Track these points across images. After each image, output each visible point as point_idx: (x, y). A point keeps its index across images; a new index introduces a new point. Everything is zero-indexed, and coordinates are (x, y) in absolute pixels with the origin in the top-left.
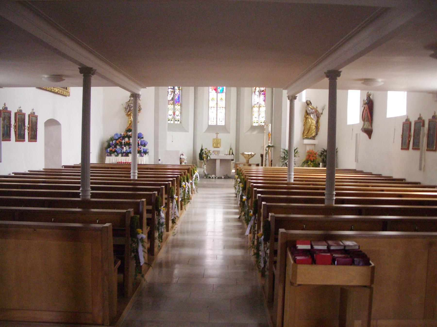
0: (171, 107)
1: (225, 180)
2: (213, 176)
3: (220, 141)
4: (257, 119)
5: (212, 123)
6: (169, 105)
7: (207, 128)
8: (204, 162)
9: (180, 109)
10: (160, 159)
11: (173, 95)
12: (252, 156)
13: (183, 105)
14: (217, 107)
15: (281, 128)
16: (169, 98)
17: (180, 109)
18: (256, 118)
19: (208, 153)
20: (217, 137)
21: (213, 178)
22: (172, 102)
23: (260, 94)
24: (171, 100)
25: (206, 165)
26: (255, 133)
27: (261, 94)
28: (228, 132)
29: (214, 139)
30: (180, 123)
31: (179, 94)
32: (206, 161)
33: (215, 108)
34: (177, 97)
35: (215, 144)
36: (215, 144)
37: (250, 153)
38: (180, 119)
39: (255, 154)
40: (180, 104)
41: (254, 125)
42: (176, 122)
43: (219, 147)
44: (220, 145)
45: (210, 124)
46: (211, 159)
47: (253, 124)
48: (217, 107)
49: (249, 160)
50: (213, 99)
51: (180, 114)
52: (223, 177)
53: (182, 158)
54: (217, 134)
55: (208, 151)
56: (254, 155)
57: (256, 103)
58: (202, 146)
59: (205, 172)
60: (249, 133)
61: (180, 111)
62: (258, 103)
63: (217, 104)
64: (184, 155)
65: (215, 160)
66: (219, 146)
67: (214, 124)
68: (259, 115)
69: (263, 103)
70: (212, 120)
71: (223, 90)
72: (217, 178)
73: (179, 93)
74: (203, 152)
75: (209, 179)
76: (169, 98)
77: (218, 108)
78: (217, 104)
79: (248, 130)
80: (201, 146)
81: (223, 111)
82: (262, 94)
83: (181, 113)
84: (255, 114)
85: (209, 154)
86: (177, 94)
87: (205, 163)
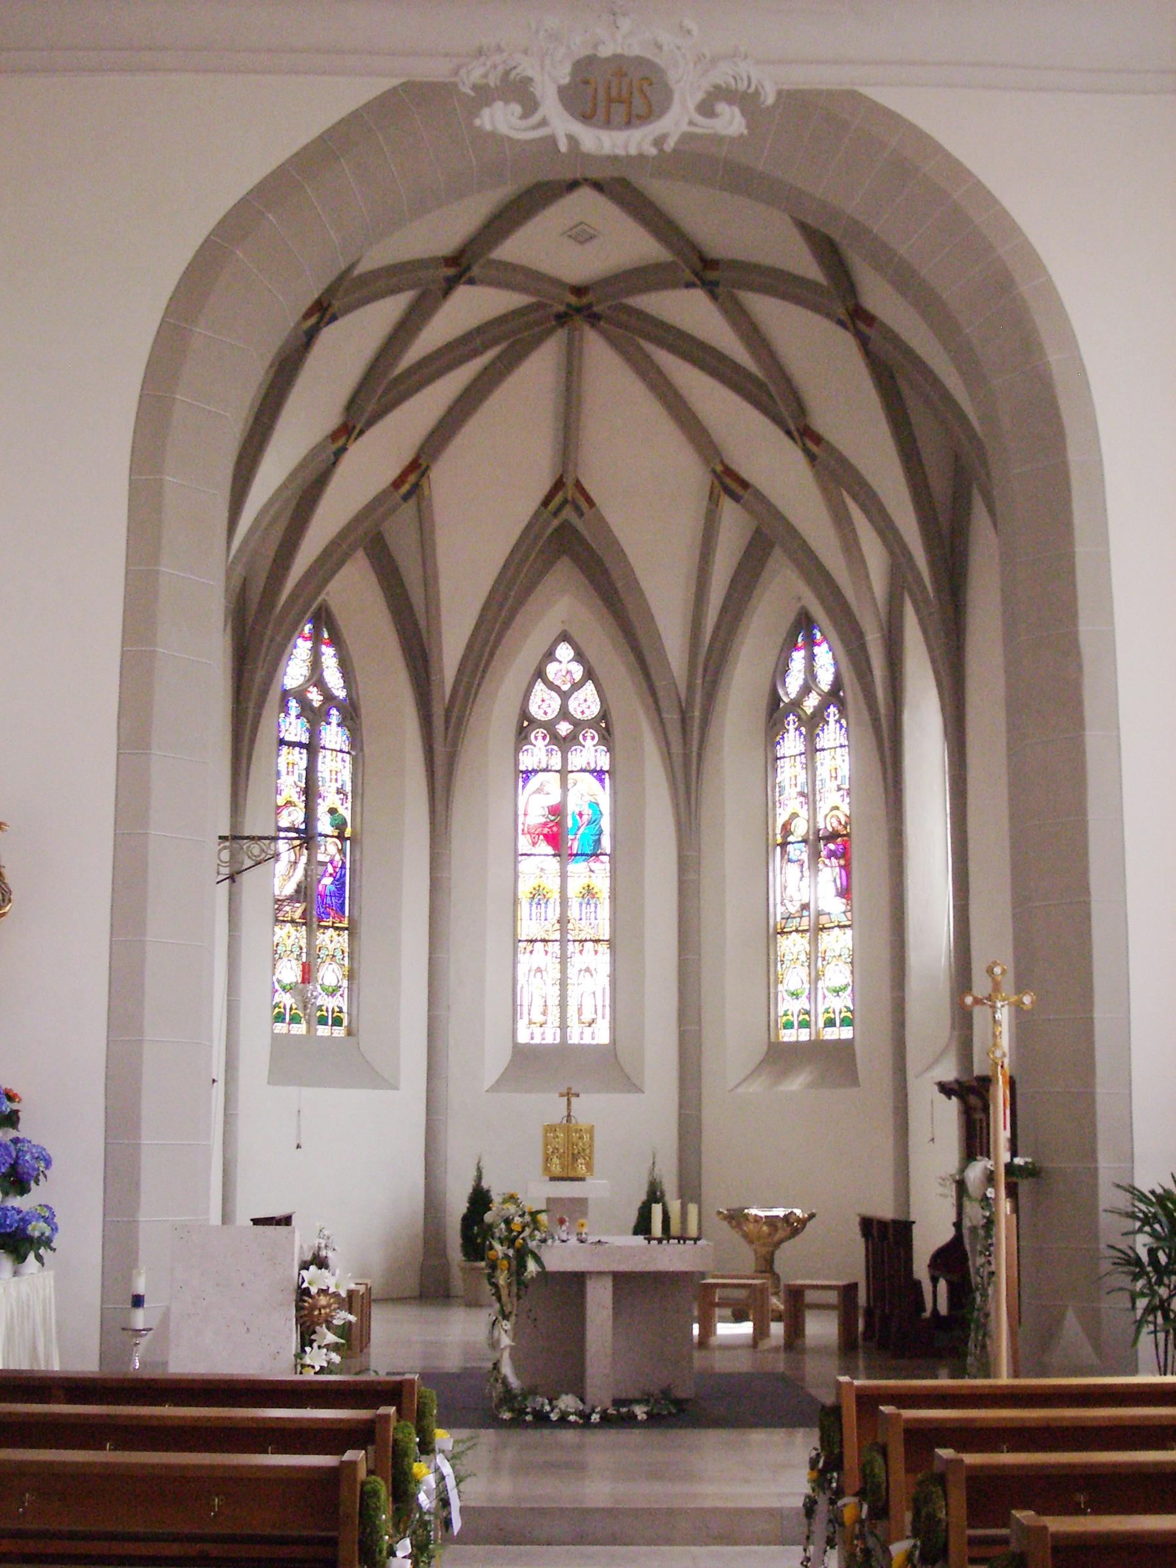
0: (290, 937)
1: (655, 1436)
2: (567, 1402)
3: (586, 1137)
4: (803, 1003)
5: (538, 1031)
6: (277, 929)
7: (509, 1058)
8: (499, 1299)
9: (346, 955)
10: (141, 1290)
11: (306, 870)
12: (793, 1227)
13: (364, 929)
14: (563, 942)
15: (1090, 1022)
16: (282, 887)
17: (346, 950)
18: (795, 995)
19: (527, 1231)
20: (569, 1115)
21: (563, 1421)
22: (299, 908)
23: (815, 855)
24: (291, 899)
25: (513, 1318)
26: (796, 1083)
27: (824, 853)
28: (633, 1087)
29: (551, 1129)
30: (349, 1033)
31: (344, 863)
32: (514, 1289)
33: (555, 948)
34: (331, 879)
35: (556, 1160)
36: (556, 1160)
37: (780, 1212)
38: (345, 1009)
39: (812, 1216)
40: (345, 924)
41: (788, 1036)
42: (323, 1031)
43: (582, 1179)
44: (589, 1167)
45: (523, 1038)
46: (545, 1276)
47: (777, 1035)
48: (563, 942)
49: (772, 1254)
50: (538, 896)
51: (345, 983)
52: (640, 1411)
53: (314, 1290)
54: (569, 1095)
55: (527, 1218)
56: (803, 1222)
57: (793, 909)
58: (479, 1170)
59: (507, 1369)
60: (757, 1087)
61: (346, 962)
62: (805, 907)
63: (563, 921)
64: (331, 1263)
65: (576, 1281)
66: (582, 1169)
67: (551, 1036)
68: (818, 978)
69: (835, 907)
70: (537, 1017)
71: (598, 842)
72: (595, 1418)
73: (338, 858)
74: (490, 1227)
75: (533, 1435)
76: (282, 887)
77: (571, 948)
78: (563, 921)
79: (756, 1071)
80: (474, 1173)
81: (601, 961)
82: (831, 854)
83: (351, 976)
84: (794, 977)
85: (532, 1236)
86: (331, 862)
87: (508, 1309)
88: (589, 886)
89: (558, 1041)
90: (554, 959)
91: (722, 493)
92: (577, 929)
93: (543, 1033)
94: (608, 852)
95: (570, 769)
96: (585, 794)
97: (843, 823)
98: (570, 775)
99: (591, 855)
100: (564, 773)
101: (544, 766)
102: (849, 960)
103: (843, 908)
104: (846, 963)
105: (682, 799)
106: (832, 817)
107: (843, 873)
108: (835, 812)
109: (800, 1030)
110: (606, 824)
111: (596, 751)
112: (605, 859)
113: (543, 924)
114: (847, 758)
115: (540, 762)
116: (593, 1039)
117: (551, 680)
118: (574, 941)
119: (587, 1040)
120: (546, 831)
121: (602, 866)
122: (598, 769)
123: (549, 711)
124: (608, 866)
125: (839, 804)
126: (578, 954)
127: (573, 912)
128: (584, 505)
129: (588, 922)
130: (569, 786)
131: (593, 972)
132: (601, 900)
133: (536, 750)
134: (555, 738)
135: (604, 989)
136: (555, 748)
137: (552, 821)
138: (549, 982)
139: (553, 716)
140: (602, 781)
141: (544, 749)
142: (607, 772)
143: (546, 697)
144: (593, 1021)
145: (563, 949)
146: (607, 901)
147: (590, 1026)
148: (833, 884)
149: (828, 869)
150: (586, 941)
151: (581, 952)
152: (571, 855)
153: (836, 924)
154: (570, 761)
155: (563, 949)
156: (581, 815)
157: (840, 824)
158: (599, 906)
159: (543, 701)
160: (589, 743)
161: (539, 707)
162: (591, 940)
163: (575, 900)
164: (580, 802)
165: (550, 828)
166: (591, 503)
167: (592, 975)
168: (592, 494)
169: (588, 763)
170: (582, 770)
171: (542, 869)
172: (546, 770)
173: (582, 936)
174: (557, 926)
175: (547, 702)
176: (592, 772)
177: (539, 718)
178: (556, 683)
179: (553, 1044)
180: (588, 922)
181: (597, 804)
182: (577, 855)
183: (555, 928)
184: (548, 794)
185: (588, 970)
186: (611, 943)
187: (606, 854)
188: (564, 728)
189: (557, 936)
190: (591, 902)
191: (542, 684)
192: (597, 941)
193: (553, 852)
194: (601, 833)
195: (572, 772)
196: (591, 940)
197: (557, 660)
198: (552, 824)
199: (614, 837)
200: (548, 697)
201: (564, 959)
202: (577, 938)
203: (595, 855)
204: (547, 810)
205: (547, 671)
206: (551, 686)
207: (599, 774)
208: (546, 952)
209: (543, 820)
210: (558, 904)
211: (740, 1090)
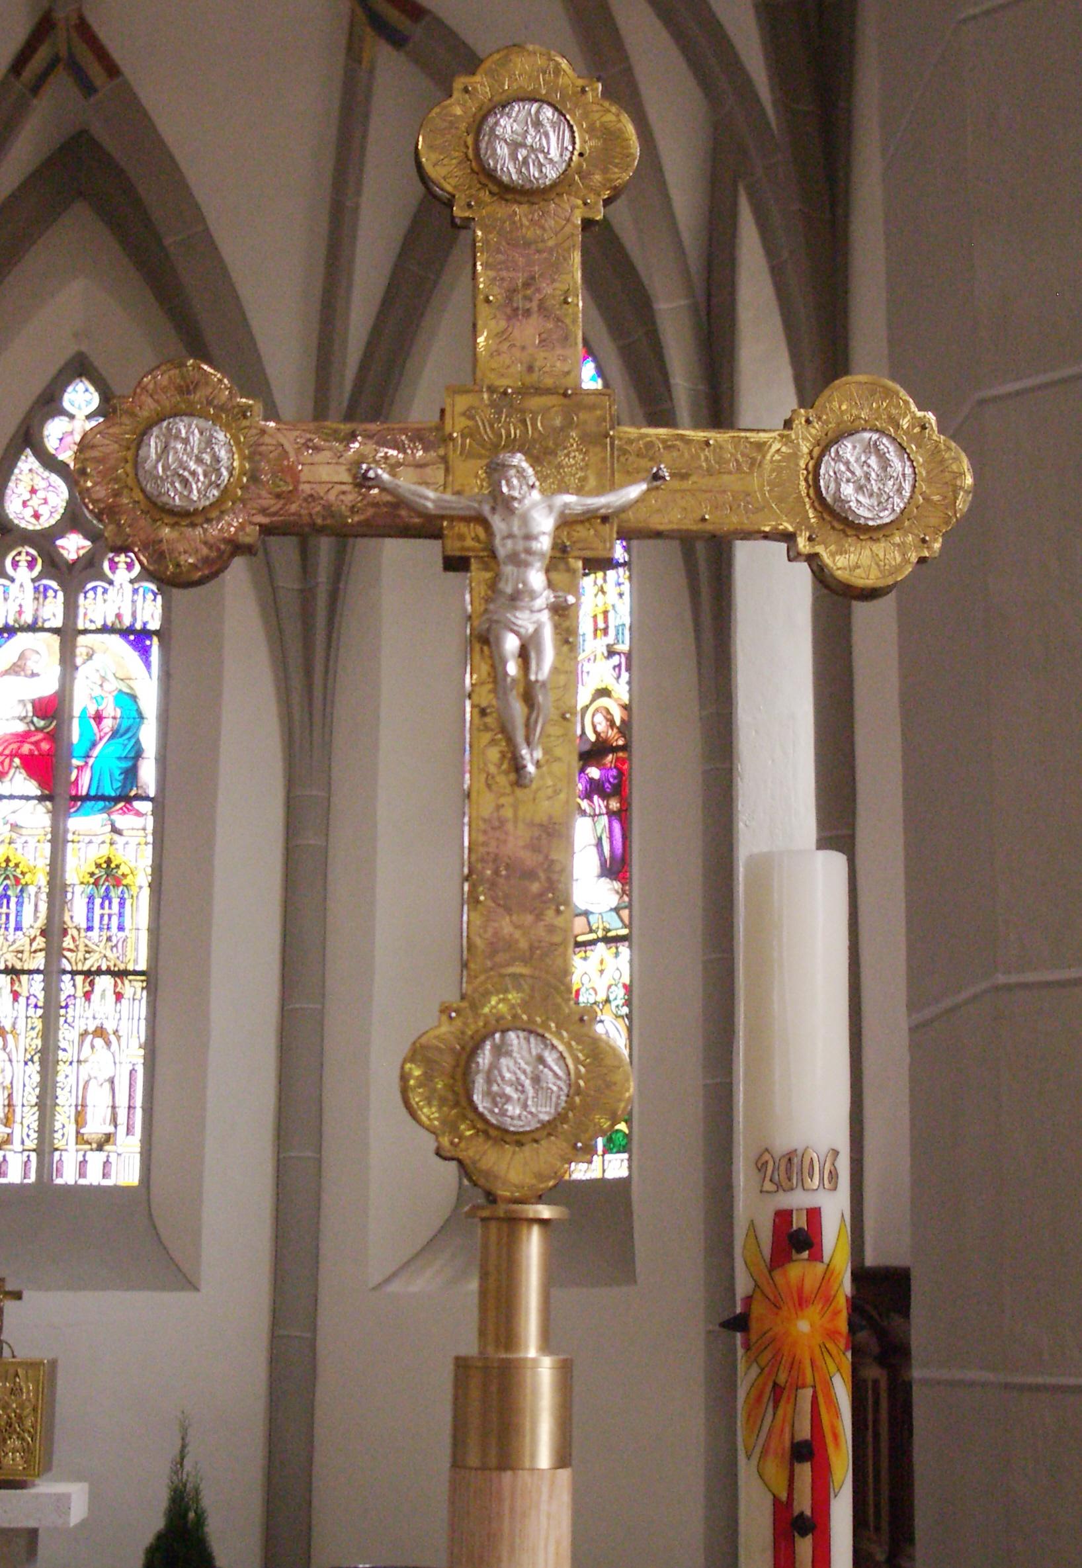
14: (51, 974)
63: (54, 931)
71: (131, 774)
78: (54, 931)
88: (109, 861)
89: (32, 1179)
90: (31, 1011)
91: (369, 32)
92: (82, 948)
93: (107, 1163)
94: (152, 794)
95: (81, 626)
96: (110, 677)
97: (618, 723)
98: (81, 640)
99: (116, 800)
100: (68, 634)
101: (28, 618)
102: (625, 1010)
103: (614, 900)
104: (617, 1016)
105: (297, 683)
106: (597, 710)
107: (617, 827)
108: (603, 702)
109: (607, 1157)
110: (149, 736)
111: (135, 591)
112: (145, 807)
113: (11, 938)
114: (626, 588)
115: (20, 613)
116: (105, 1175)
117: (53, 451)
118: (74, 973)
119: (94, 1177)
120: (26, 748)
121: (138, 822)
122: (138, 626)
123: (44, 511)
124: (150, 822)
125: (609, 683)
126: (80, 1001)
127: (77, 912)
128: (95, 71)
129: (105, 934)
130: (79, 661)
131: (113, 1038)
132: (134, 890)
133: (14, 588)
134: (54, 566)
135: (132, 1072)
136: (54, 584)
137: (38, 730)
138: (20, 1056)
139: (53, 522)
140: (145, 652)
141: (29, 587)
142: (156, 633)
143: (40, 484)
144: (108, 1138)
145: (51, 990)
146: (145, 894)
147: (100, 1148)
148: (594, 850)
149: (587, 821)
150: (99, 972)
151: (87, 995)
152: (76, 798)
153: (600, 934)
154: (81, 611)
155: (51, 990)
156: (99, 718)
157: (612, 723)
158: (128, 903)
159: (33, 491)
160: (122, 576)
161: (25, 504)
162: (109, 972)
163: (79, 889)
164: (97, 692)
165: (36, 744)
166: (112, 70)
167: (108, 1044)
168: (117, 55)
169: (118, 616)
170: (105, 629)
171: (15, 827)
172: (33, 628)
173: (92, 963)
174: (40, 942)
175: (41, 494)
176: (125, 633)
177: (23, 525)
178: (61, 457)
179: (22, 1186)
180: (105, 934)
181: (134, 698)
182: (87, 798)
183: (35, 946)
184: (33, 675)
185: (100, 1032)
186: (151, 978)
187: (147, 798)
188: (73, 546)
189: (39, 962)
190: (112, 894)
191: (32, 459)
192: (120, 974)
193: (39, 793)
194: (138, 754)
195: (85, 632)
196: (109, 972)
197: (64, 413)
198: (40, 736)
199: (162, 761)
200: (43, 484)
201: (51, 1011)
202: (80, 968)
203: (124, 798)
204: (30, 707)
205: (46, 433)
206: (50, 462)
207: (138, 638)
208: (16, 995)
209: (21, 727)
210: (44, 897)
211: (394, 1287)
